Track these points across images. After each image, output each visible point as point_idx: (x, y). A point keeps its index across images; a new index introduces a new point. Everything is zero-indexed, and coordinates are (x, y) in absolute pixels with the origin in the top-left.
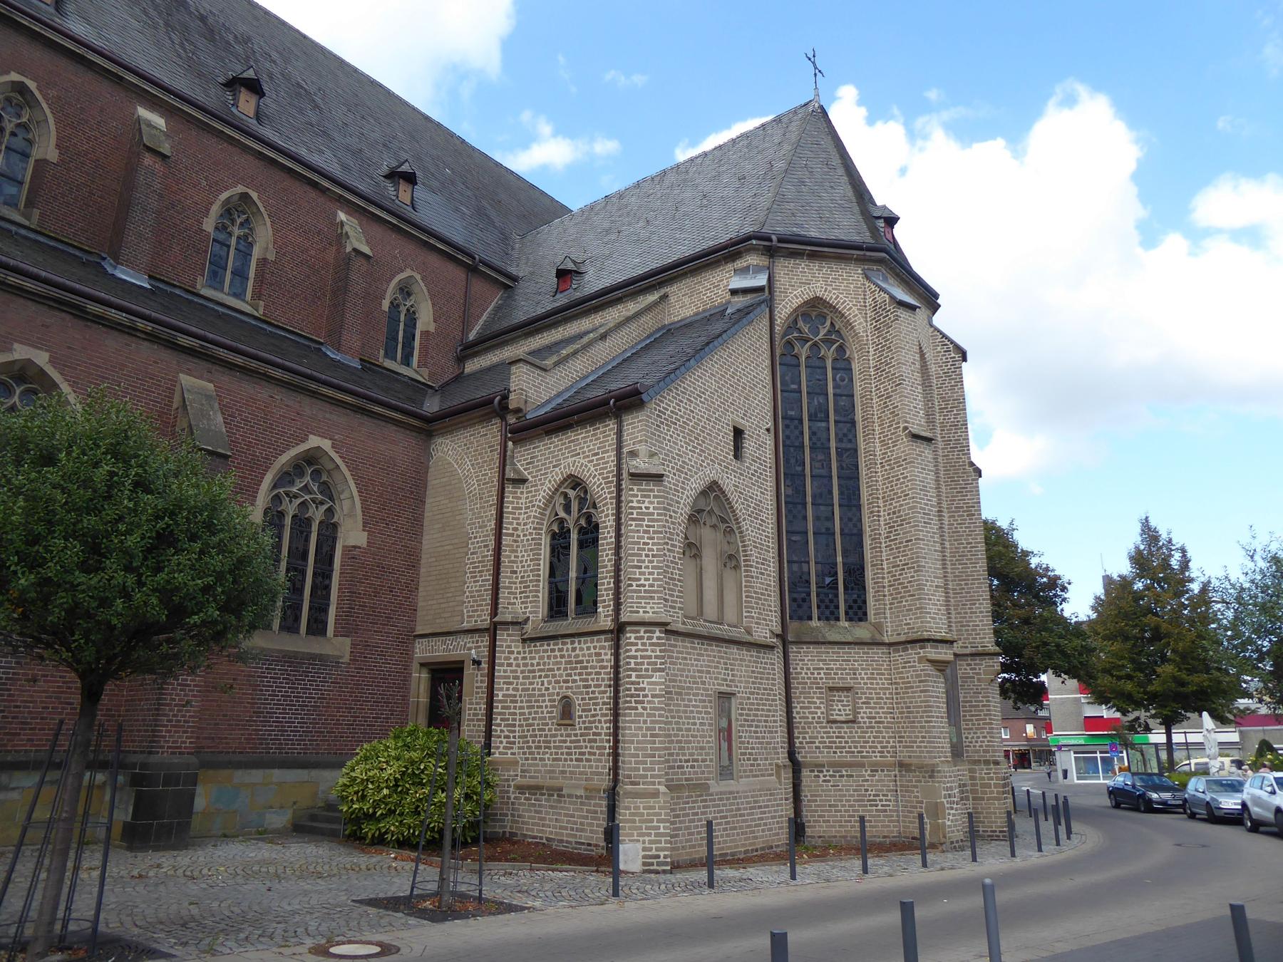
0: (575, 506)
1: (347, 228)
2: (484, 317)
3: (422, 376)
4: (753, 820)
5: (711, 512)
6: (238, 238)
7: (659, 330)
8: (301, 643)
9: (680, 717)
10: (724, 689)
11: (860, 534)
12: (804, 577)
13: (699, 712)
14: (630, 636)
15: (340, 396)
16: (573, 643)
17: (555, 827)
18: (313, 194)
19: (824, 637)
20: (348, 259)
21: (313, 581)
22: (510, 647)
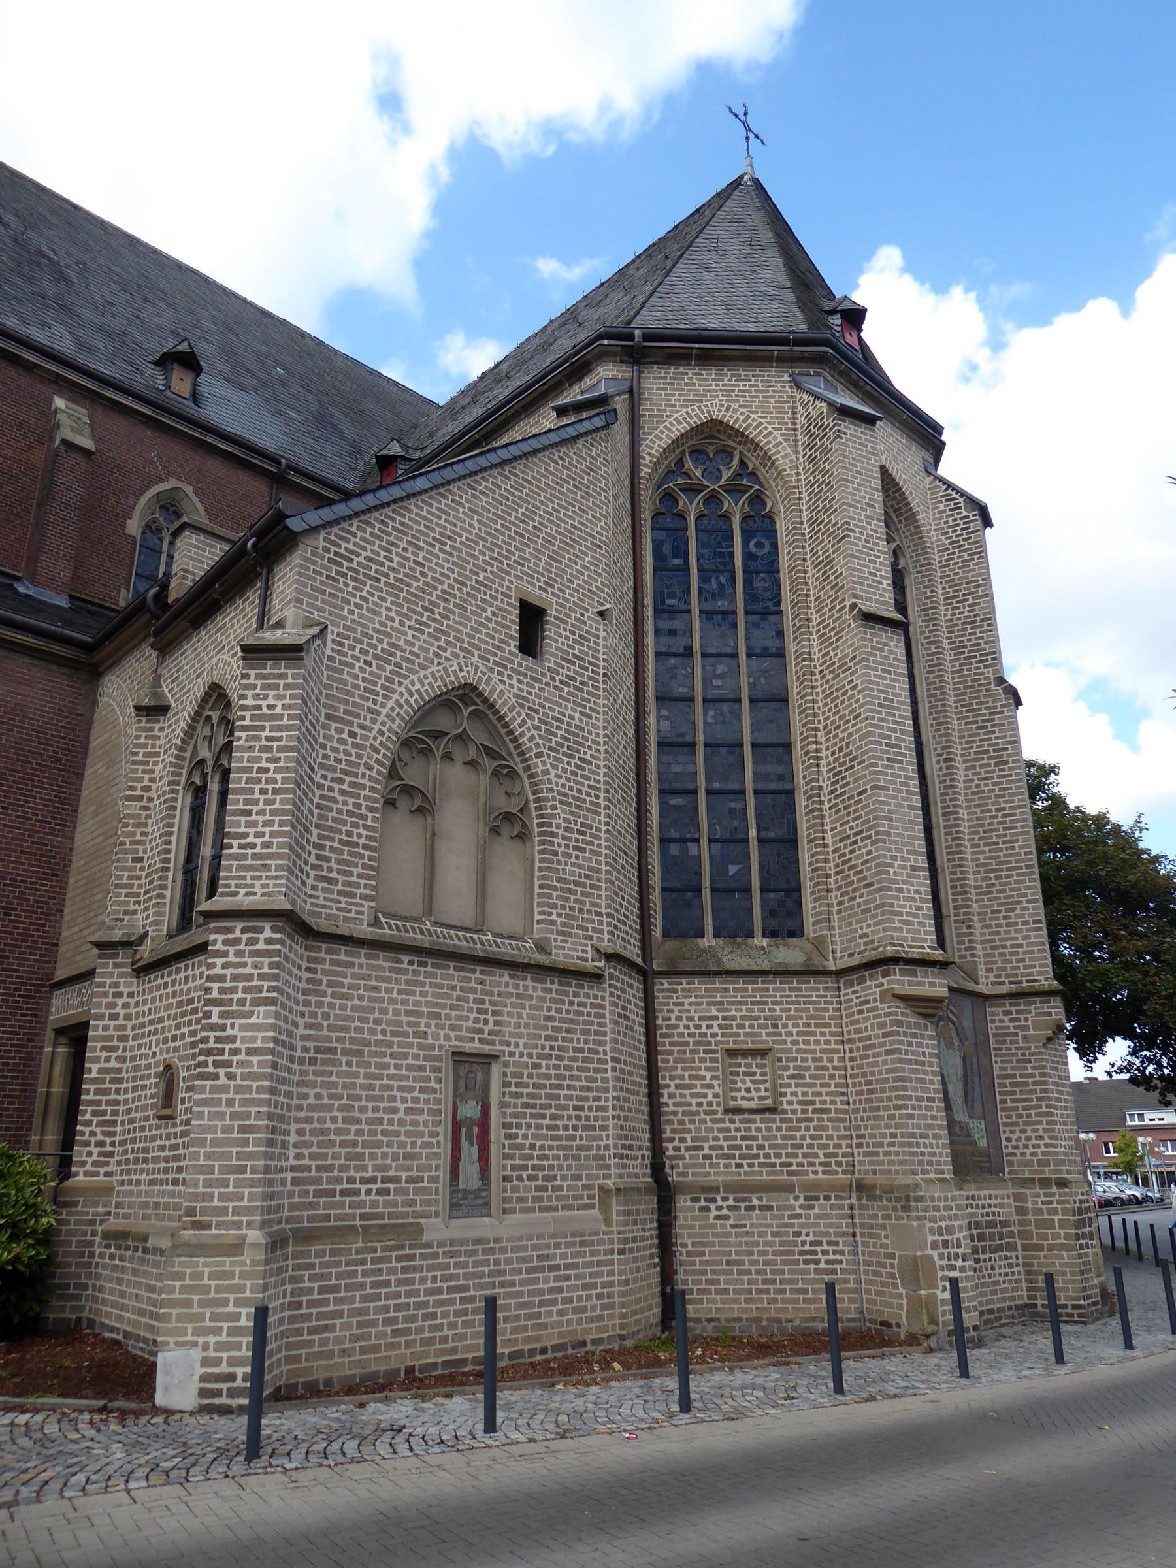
5: (463, 738)
15: (20, 637)
19: (719, 962)
22: (116, 985)
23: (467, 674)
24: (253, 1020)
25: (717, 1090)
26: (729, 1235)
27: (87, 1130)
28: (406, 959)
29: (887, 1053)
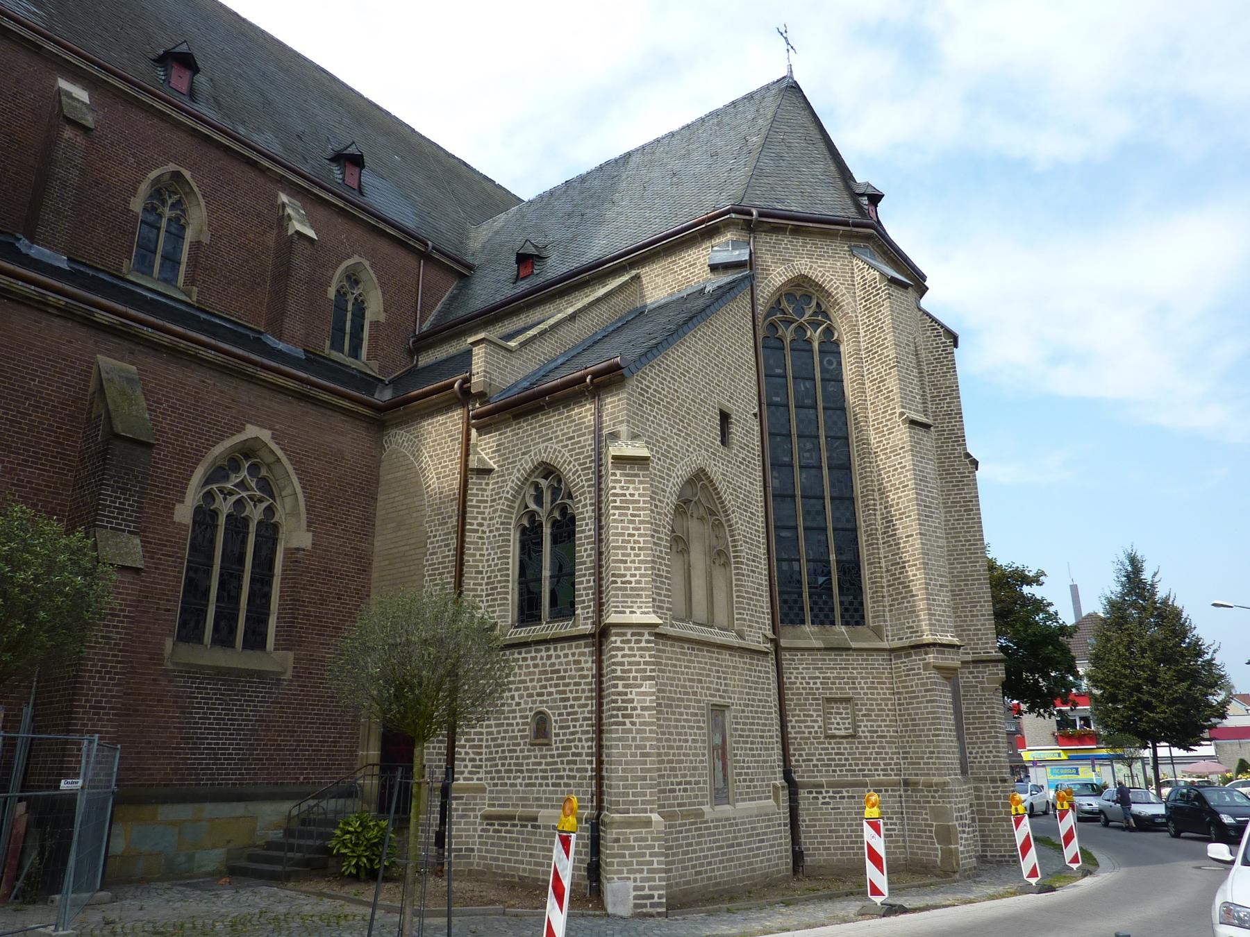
0: (547, 497)
1: (289, 211)
2: (438, 308)
3: (373, 369)
4: (750, 850)
6: (169, 220)
7: (630, 312)
8: (237, 658)
9: (671, 733)
10: (717, 700)
11: (854, 530)
12: (796, 576)
13: (691, 728)
14: (616, 640)
16: (548, 650)
17: (529, 863)
18: (252, 174)
20: (290, 240)
21: (251, 588)
23: (700, 462)
24: (643, 689)
25: (821, 724)
26: (830, 814)
27: (463, 751)
28: (686, 646)
29: (928, 702)
